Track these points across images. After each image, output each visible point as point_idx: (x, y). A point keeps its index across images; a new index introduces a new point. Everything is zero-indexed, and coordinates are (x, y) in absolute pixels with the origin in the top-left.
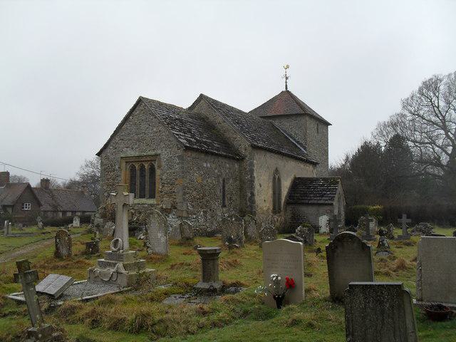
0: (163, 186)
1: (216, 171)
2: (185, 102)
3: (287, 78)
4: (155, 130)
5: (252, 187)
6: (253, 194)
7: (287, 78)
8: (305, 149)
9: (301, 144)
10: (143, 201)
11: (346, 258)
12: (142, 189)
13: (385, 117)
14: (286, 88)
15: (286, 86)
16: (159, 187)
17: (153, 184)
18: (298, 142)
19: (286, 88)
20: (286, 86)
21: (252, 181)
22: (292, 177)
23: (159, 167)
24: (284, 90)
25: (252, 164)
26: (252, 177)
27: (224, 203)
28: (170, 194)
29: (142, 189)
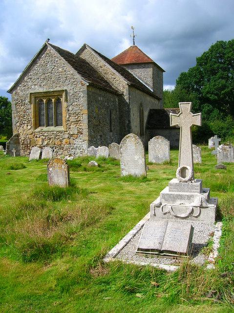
5: (129, 116)
6: (129, 121)
16: (65, 115)
18: (146, 83)
19: (134, 44)
21: (129, 112)
22: (148, 109)
27: (111, 129)
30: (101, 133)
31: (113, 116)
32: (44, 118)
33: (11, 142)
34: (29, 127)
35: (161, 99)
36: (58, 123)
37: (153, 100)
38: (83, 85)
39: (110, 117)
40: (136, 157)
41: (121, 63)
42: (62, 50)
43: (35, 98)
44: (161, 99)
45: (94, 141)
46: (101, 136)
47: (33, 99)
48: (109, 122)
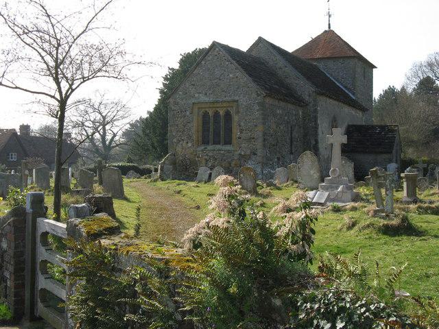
0: (241, 133)
1: (286, 118)
2: (243, 44)
3: (330, 16)
4: (231, 76)
5: (316, 134)
6: (317, 142)
7: (330, 16)
8: (354, 94)
9: (348, 89)
10: (218, 147)
11: (114, 247)
12: (217, 134)
13: (178, 60)
14: (329, 27)
15: (329, 24)
16: (236, 133)
17: (229, 130)
18: (346, 87)
19: (329, 27)
20: (329, 24)
21: (316, 128)
22: (346, 124)
23: (238, 112)
24: (327, 29)
25: (316, 111)
26: (316, 124)
27: (291, 150)
28: (250, 139)
29: (217, 134)
30: (278, 155)
31: (295, 134)
32: (211, 137)
33: (166, 162)
34: (190, 145)
35: (367, 110)
36: (228, 142)
37: (353, 111)
38: (258, 95)
39: (291, 135)
40: (312, 172)
41: (309, 56)
42: (230, 48)
43: (199, 108)
44: (367, 110)
45: (192, 320)
46: (278, 159)
47: (196, 110)
48: (288, 141)
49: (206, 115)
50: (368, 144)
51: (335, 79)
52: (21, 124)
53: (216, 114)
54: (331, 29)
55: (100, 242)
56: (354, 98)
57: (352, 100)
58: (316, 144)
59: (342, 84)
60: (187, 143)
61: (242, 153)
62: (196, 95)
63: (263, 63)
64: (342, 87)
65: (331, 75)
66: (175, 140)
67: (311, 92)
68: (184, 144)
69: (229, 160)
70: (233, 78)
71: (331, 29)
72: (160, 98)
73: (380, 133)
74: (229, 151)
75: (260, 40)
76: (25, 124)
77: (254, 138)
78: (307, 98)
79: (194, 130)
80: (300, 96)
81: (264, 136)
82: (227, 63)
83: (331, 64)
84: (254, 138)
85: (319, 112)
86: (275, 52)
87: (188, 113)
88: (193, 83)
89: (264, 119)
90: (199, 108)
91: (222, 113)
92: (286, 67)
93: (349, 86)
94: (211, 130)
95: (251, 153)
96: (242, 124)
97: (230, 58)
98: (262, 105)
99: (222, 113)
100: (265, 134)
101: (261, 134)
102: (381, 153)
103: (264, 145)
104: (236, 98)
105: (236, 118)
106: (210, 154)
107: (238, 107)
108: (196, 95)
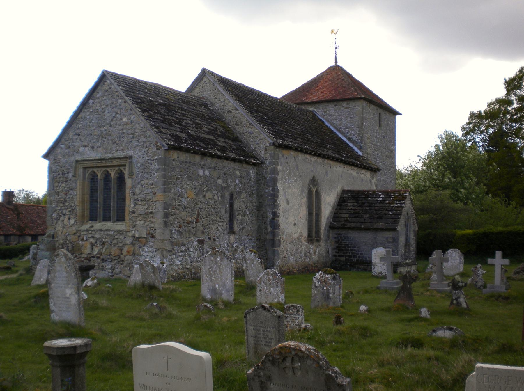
0: (136, 204)
1: (220, 181)
8: (360, 148)
12: (107, 208)
15: (336, 59)
16: (130, 205)
18: (350, 139)
23: (131, 174)
25: (275, 172)
28: (148, 214)
29: (107, 208)
34: (72, 221)
36: (121, 218)
37: (353, 172)
38: (158, 148)
43: (85, 168)
47: (80, 171)
49: (93, 178)
50: (365, 216)
51: (337, 129)
52: (4, 190)
53: (107, 177)
54: (338, 64)
55: (408, 269)
56: (360, 153)
57: (357, 157)
58: (273, 219)
59: (345, 136)
60: (69, 219)
61: (137, 236)
62: (81, 149)
63: (206, 106)
64: (344, 139)
65: (332, 124)
66: (55, 215)
67: (267, 145)
68: (66, 222)
69: (120, 245)
70: (127, 124)
71: (338, 64)
72: (419, 166)
73: (383, 201)
74: (119, 232)
75: (204, 73)
76: (8, 190)
77: (151, 213)
78: (263, 152)
79: (77, 199)
80: (254, 150)
81: (165, 208)
82: (120, 101)
83: (331, 109)
84: (151, 213)
85: (280, 174)
86: (221, 89)
87: (70, 175)
88: (78, 131)
89: (165, 183)
90: (85, 168)
91: (113, 174)
92: (237, 109)
93: (354, 138)
94: (98, 202)
95: (148, 234)
96: (137, 191)
97: (123, 94)
98: (164, 163)
99: (113, 174)
100: (166, 206)
101: (160, 206)
102: (382, 230)
103: (166, 224)
104: (130, 153)
105: (129, 182)
106: (97, 236)
107: (131, 163)
108: (81, 149)
